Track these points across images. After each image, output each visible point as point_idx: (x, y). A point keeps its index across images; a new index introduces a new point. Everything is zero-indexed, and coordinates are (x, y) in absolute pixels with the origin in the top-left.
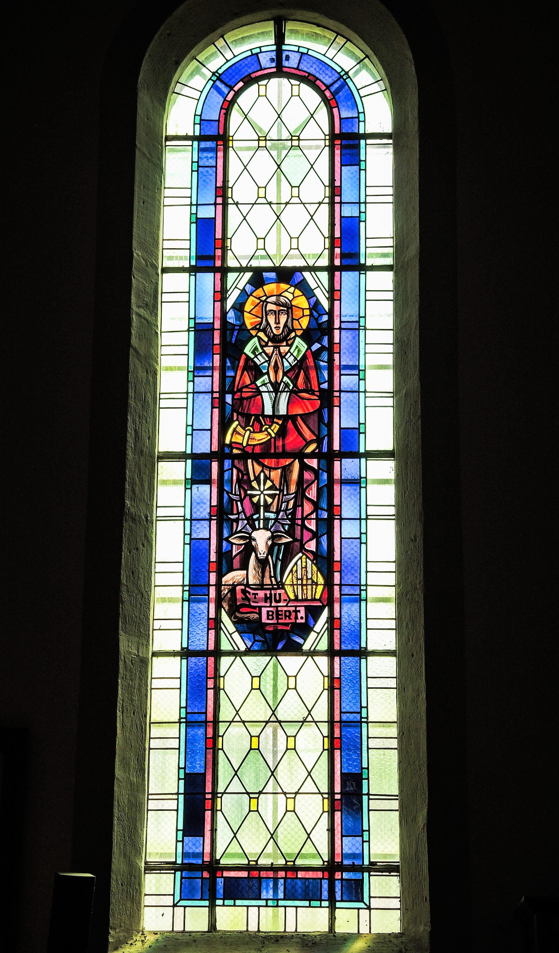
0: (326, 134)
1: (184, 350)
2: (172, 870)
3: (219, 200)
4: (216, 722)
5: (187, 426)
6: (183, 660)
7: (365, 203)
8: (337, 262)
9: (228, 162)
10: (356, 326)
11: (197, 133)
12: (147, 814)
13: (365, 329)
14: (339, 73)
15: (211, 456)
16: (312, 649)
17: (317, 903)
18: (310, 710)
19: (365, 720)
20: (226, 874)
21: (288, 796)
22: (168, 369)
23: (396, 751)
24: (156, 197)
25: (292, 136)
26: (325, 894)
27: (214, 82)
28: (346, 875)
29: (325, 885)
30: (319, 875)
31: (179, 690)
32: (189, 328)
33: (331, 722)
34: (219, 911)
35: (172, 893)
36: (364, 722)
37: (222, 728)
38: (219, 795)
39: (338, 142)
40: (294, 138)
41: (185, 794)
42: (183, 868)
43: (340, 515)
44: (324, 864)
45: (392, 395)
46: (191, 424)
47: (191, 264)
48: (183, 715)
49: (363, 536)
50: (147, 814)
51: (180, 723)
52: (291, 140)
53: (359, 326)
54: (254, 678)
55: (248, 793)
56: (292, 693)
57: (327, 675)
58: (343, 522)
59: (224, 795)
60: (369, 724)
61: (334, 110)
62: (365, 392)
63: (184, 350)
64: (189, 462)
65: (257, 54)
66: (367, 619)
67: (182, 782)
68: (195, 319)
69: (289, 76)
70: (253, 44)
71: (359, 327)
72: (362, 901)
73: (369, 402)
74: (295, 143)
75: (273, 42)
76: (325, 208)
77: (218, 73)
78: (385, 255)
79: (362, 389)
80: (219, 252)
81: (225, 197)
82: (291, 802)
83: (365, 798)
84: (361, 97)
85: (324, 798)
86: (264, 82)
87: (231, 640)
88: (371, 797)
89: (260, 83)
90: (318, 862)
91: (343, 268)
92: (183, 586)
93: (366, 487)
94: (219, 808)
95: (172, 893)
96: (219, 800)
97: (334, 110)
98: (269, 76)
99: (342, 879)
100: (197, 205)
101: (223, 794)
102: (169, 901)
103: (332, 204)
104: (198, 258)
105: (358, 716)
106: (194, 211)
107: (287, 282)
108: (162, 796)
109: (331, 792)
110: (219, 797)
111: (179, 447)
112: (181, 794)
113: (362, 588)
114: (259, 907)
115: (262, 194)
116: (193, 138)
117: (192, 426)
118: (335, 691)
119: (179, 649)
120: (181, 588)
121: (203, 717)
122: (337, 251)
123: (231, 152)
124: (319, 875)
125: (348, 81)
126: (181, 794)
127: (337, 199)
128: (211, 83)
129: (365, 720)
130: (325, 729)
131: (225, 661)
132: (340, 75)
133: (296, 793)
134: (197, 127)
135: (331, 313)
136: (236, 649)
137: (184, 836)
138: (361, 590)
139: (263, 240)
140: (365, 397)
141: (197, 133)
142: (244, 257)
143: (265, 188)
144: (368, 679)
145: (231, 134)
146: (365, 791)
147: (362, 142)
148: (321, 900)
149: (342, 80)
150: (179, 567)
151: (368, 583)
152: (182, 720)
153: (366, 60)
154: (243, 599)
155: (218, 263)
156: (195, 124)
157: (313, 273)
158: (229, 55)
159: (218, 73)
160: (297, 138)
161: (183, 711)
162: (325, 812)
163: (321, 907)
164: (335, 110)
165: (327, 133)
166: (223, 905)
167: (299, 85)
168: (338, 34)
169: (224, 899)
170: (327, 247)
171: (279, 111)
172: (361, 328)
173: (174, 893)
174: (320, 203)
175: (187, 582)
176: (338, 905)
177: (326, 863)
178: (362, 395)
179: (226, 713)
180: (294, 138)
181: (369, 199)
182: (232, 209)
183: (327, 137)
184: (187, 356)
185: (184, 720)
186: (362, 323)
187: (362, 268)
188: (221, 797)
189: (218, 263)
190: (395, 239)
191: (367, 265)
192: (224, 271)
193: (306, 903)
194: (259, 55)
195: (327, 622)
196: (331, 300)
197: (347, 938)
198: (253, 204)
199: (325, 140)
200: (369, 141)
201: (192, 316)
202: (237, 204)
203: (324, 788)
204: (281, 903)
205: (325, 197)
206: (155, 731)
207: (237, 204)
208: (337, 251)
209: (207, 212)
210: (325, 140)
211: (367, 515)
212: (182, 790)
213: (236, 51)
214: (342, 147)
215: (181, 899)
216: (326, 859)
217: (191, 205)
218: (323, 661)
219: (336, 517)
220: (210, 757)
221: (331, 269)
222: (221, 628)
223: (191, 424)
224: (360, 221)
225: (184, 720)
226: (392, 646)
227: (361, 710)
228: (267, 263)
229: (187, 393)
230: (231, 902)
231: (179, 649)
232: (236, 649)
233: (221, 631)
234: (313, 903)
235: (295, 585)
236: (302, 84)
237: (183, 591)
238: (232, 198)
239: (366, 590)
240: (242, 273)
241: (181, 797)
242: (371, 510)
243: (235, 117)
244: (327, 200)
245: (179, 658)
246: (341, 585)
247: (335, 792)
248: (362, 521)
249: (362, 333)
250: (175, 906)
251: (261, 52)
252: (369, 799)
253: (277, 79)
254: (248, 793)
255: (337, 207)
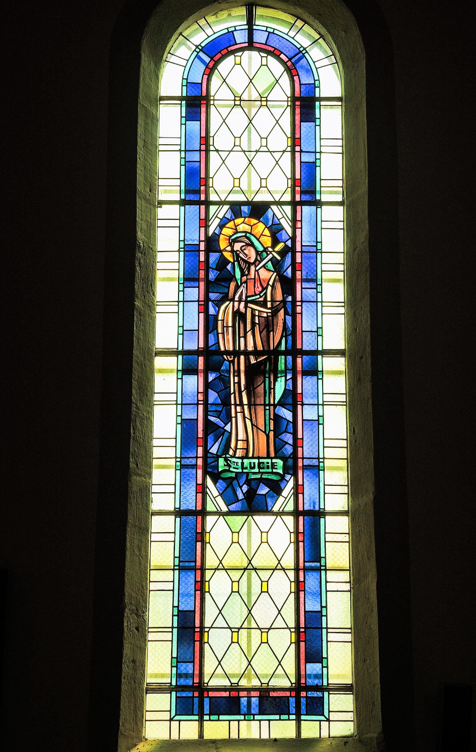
0: (288, 96)
1: (176, 266)
2: (169, 691)
3: (203, 147)
4: (203, 569)
5: (179, 327)
6: (177, 519)
7: (320, 152)
8: (298, 198)
9: (210, 125)
10: (314, 249)
11: (184, 94)
12: (151, 544)
13: (326, 570)
14: (299, 49)
15: (197, 353)
16: (281, 510)
17: (286, 717)
18: (280, 666)
19: (324, 568)
20: (211, 694)
21: (262, 630)
22: (161, 371)
23: (352, 713)
24: (153, 134)
25: (261, 97)
26: (293, 710)
27: (198, 53)
28: (310, 694)
29: (292, 700)
30: (288, 694)
31: (174, 486)
32: (180, 248)
33: (297, 569)
34: (206, 724)
35: (172, 580)
36: (323, 570)
37: (208, 574)
38: (207, 630)
39: (298, 103)
40: (263, 99)
41: (178, 628)
42: (178, 688)
43: (302, 401)
44: (292, 686)
45: (343, 304)
46: (177, 605)
47: (182, 198)
48: (177, 563)
49: (321, 419)
50: (151, 544)
51: (179, 251)
52: (261, 101)
53: (317, 250)
54: (236, 139)
55: (230, 628)
56: (265, 545)
57: (290, 178)
58: (304, 406)
59: (211, 629)
60: (323, 254)
61: (295, 77)
62: (322, 302)
63: (176, 266)
64: (180, 357)
65: (232, 32)
66: (325, 493)
67: (176, 618)
68: (184, 241)
69: (260, 50)
70: (230, 24)
71: (317, 251)
72: (323, 715)
73: (325, 310)
74: (264, 103)
75: (245, 23)
76: (288, 156)
77: (201, 46)
78: (336, 193)
79: (319, 299)
80: (203, 188)
81: (207, 144)
82: (235, 635)
83: (324, 631)
84: (317, 69)
85: (291, 632)
86: (240, 54)
87: (215, 504)
88: (329, 630)
89: (235, 55)
90: (287, 684)
91: (302, 203)
92: (176, 457)
93: (322, 379)
94: (206, 641)
95: (179, 178)
96: (206, 634)
97: (295, 77)
98: (242, 49)
99: (306, 697)
100: (184, 301)
101: (210, 628)
102: (166, 716)
103: (293, 152)
104: (187, 192)
105: (315, 248)
106: (183, 155)
107: (258, 218)
108: (160, 629)
109: (298, 627)
110: (206, 632)
111: (172, 344)
112: (175, 628)
113: (321, 460)
114: (239, 721)
115: (237, 184)
116: (181, 98)
117: (183, 327)
118: (300, 543)
119: (172, 509)
120: (174, 459)
121: (193, 564)
122: (298, 189)
123: (212, 108)
124: (288, 694)
125: (306, 55)
126: (175, 628)
127: (298, 148)
128: (195, 53)
129: (324, 568)
130: (292, 574)
131: (210, 520)
132: (300, 50)
133: (269, 629)
134: (185, 88)
135: (293, 239)
136: (219, 510)
137: (186, 121)
138: (319, 462)
139: (239, 179)
140: (322, 306)
141: (184, 94)
142: (223, 192)
143: (239, 179)
144: (324, 395)
145: (206, 681)
146: (324, 625)
147: (317, 103)
148: (289, 714)
149: (301, 54)
150: (177, 182)
151: (324, 300)
152: (176, 568)
153: (321, 41)
154: (225, 465)
155: (203, 197)
156: (182, 86)
157: (279, 206)
158: (209, 32)
159: (201, 46)
160: (265, 99)
161: (177, 560)
162: (292, 543)
163: (289, 719)
164: (296, 78)
165: (289, 95)
166: (210, 720)
167: (267, 57)
168: (298, 18)
169: (210, 715)
170: (289, 145)
171: (250, 565)
172: (318, 251)
173: (180, 177)
174: (284, 151)
175: (179, 455)
176: (303, 717)
177: (294, 685)
178: (319, 304)
179: (211, 561)
180: (263, 99)
181: (323, 149)
182: (213, 155)
183: (289, 99)
184: (178, 271)
185: (178, 568)
186: (319, 247)
187: (318, 204)
188: (208, 632)
189: (203, 197)
190: (351, 544)
191: (322, 200)
192: (208, 203)
193: (277, 717)
194: (234, 32)
195: (293, 488)
196: (294, 228)
197: (311, 742)
198: (230, 151)
199: (288, 101)
200: (322, 103)
201: (182, 238)
202: (217, 151)
203: (292, 624)
204: (256, 717)
205: (288, 146)
206: (154, 575)
207: (217, 151)
208: (298, 189)
209: (195, 157)
210: (288, 101)
211: (323, 402)
212: (175, 625)
213: (216, 29)
214: (302, 107)
215: (176, 714)
216: (293, 681)
217: (180, 151)
218: (290, 520)
219: (298, 403)
220: (198, 598)
221: (294, 204)
222: (207, 493)
223: (184, 157)
224: (322, 616)
225: (178, 568)
226: (344, 507)
227: (317, 244)
228: (241, 198)
229: (178, 302)
230: (215, 717)
231: (172, 509)
232: (219, 510)
233: (207, 495)
234: (283, 717)
235: (267, 405)
236: (269, 57)
237: (176, 462)
238: (213, 145)
239: (323, 462)
240: (221, 206)
241: (175, 631)
242: (327, 398)
243: (216, 81)
244: (289, 149)
245: (174, 517)
246: (302, 252)
247: (296, 150)
248: (317, 154)
249: (319, 255)
250: (171, 720)
251: (236, 30)
252: (327, 632)
253: (247, 51)
254: (230, 628)
255: (297, 155)
